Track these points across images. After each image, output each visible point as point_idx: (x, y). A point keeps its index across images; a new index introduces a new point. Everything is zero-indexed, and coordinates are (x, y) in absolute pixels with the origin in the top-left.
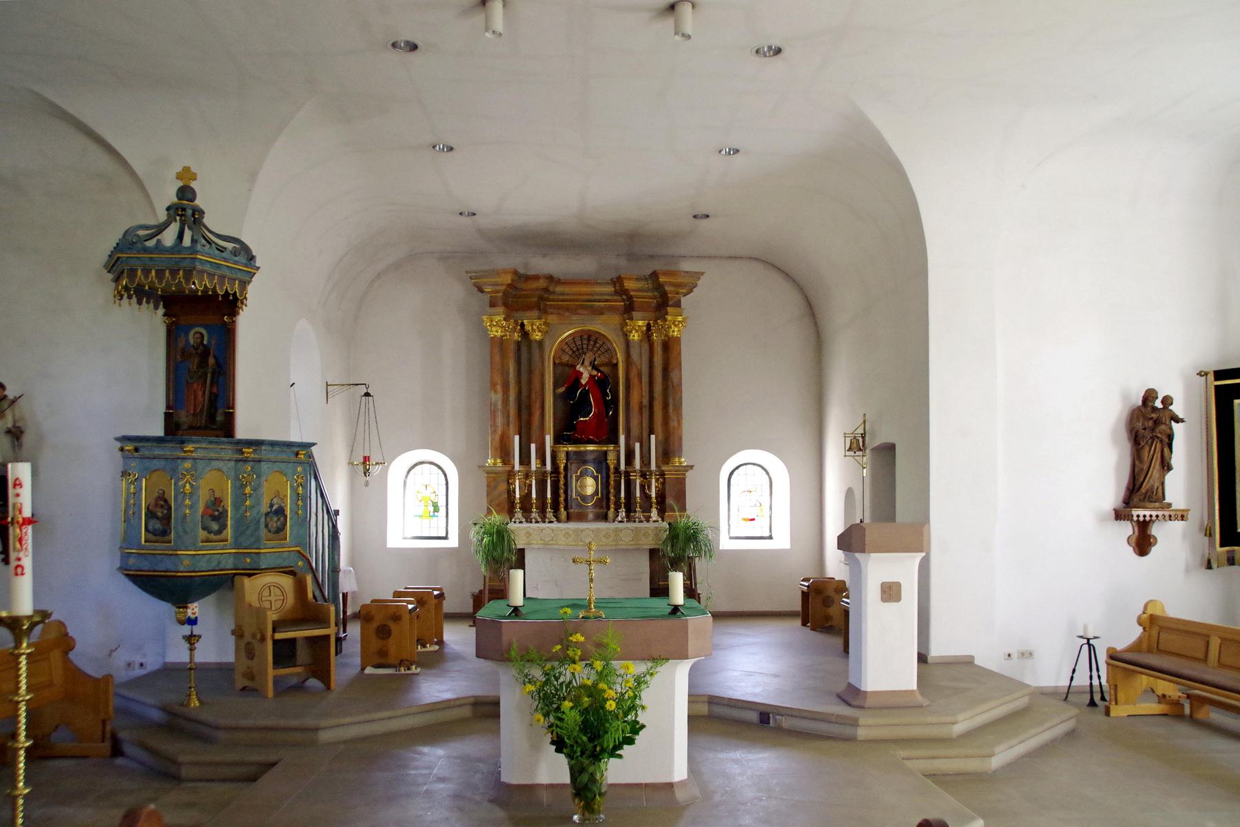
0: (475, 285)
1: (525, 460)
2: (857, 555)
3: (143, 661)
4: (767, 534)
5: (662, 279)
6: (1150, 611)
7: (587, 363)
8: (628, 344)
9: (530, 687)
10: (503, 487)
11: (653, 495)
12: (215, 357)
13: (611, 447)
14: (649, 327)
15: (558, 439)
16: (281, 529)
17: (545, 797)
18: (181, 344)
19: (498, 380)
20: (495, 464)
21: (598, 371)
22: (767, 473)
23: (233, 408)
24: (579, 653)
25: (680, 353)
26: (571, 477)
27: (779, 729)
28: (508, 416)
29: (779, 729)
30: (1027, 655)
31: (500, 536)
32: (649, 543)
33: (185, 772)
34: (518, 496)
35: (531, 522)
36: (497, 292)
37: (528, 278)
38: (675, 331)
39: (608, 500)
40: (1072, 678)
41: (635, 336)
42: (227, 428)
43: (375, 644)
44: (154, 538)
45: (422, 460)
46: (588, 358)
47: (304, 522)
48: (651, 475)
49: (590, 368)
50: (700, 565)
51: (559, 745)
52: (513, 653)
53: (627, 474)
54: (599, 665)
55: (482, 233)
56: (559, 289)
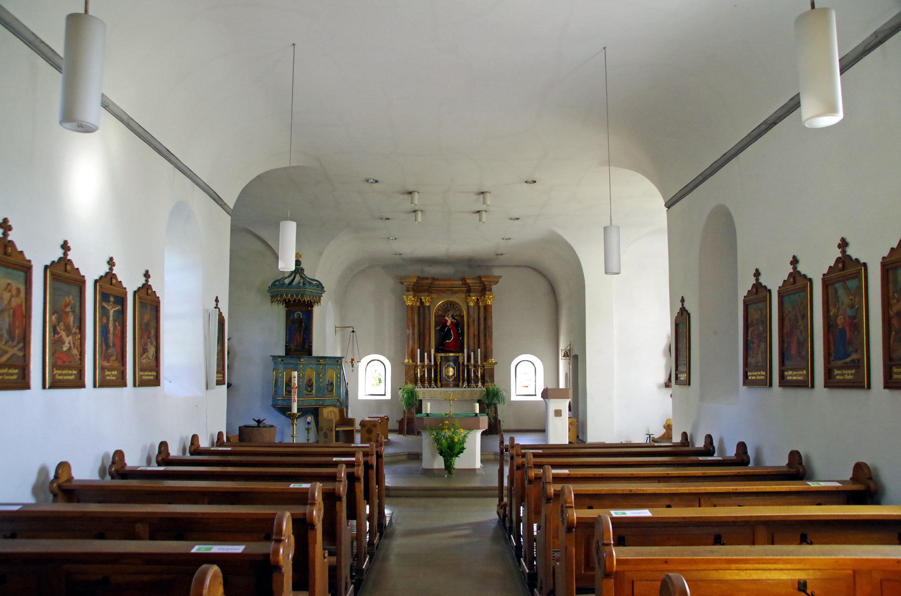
0: (400, 282)
1: (422, 360)
6: (668, 423)
7: (450, 316)
8: (468, 307)
9: (433, 436)
10: (412, 372)
11: (479, 376)
14: (478, 300)
15: (437, 351)
16: (332, 390)
17: (436, 472)
19: (410, 324)
20: (409, 361)
21: (455, 319)
22: (534, 365)
23: (312, 343)
24: (447, 427)
25: (491, 312)
28: (414, 340)
31: (412, 394)
34: (419, 376)
35: (425, 388)
36: (409, 285)
37: (424, 279)
38: (489, 302)
39: (459, 378)
41: (472, 304)
42: (309, 352)
44: (288, 394)
46: (450, 314)
47: (339, 387)
48: (478, 367)
50: (500, 407)
51: (441, 453)
52: (427, 426)
53: (468, 366)
54: (452, 430)
55: (404, 260)
56: (437, 283)
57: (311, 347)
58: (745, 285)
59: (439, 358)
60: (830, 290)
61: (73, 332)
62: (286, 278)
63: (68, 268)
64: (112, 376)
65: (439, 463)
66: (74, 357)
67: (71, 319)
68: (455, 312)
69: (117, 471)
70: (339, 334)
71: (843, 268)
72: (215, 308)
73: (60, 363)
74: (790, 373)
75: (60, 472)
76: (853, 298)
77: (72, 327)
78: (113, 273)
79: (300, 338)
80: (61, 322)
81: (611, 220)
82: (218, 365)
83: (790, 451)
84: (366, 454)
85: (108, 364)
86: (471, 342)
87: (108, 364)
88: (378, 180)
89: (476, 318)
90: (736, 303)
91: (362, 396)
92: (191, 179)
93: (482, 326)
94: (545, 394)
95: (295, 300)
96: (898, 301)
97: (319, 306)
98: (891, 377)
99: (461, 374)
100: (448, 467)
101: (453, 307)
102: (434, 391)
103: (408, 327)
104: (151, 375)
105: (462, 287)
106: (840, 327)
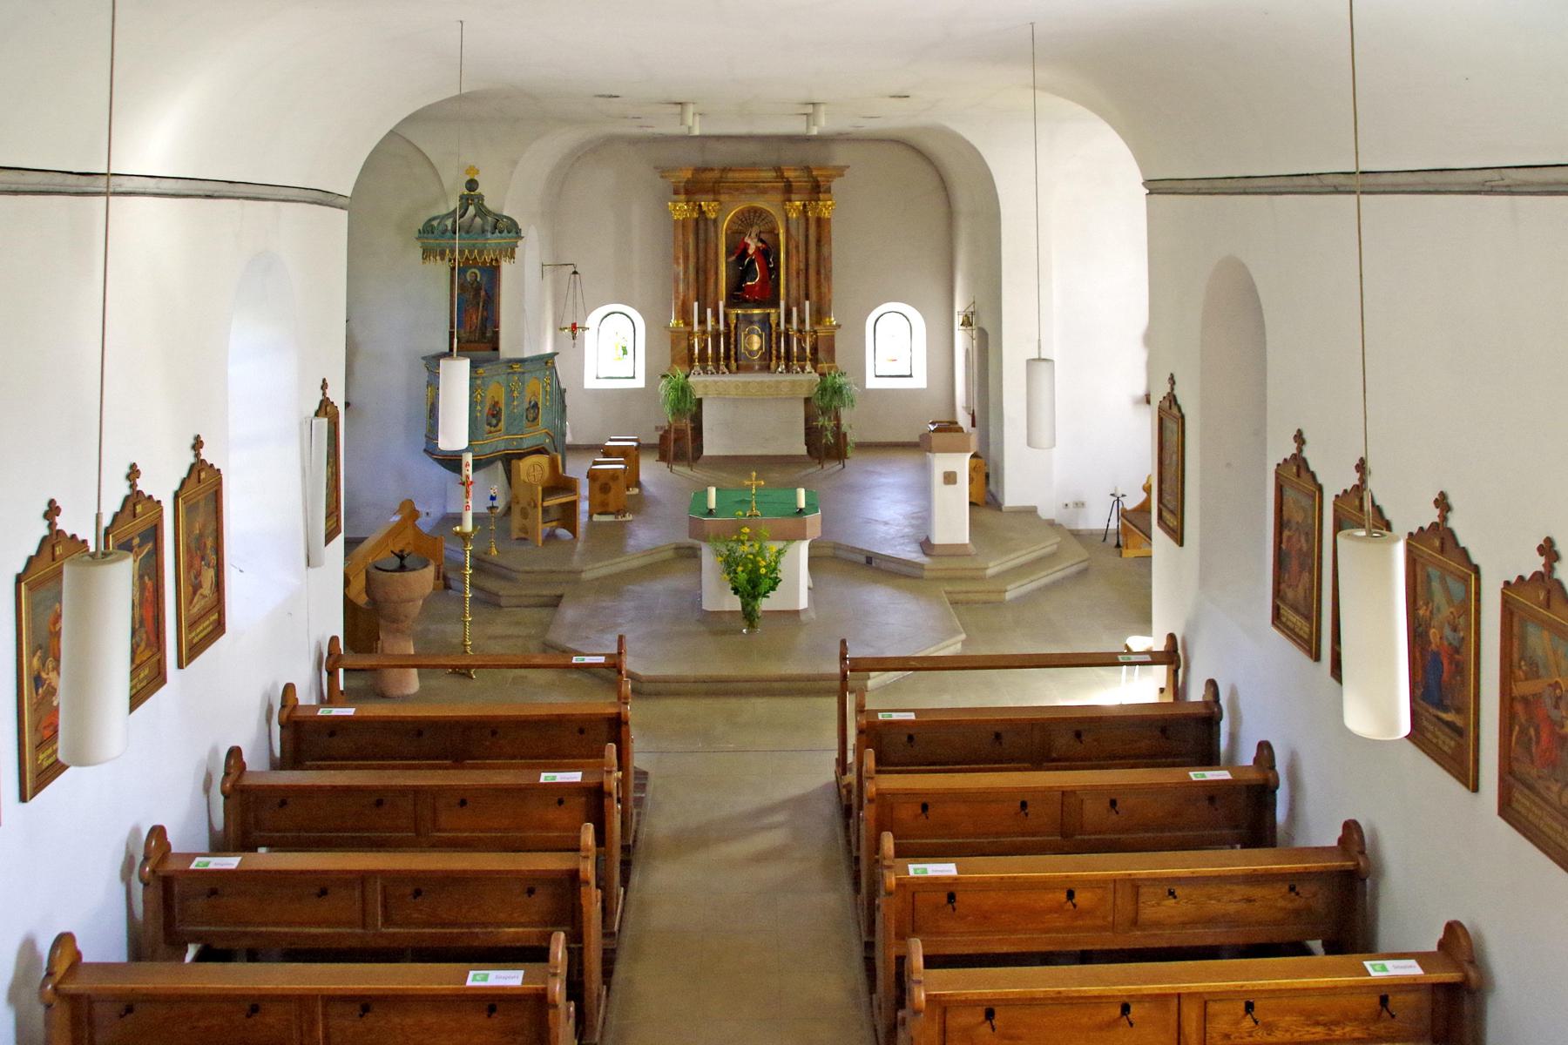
1: (702, 321)
2: (928, 454)
3: (428, 511)
4: (908, 374)
5: (815, 173)
7: (753, 235)
8: (787, 220)
10: (684, 344)
12: (486, 291)
13: (773, 311)
14: (804, 206)
15: (728, 305)
16: (535, 418)
20: (678, 324)
26: (740, 335)
27: (878, 569)
29: (878, 569)
30: (1080, 505)
31: (683, 390)
32: (804, 393)
33: (503, 602)
36: (679, 182)
38: (826, 214)
39: (771, 353)
40: (1108, 526)
43: (599, 497)
46: (755, 230)
49: (756, 240)
56: (730, 175)
59: (733, 321)
65: (734, 603)
68: (764, 225)
70: (548, 277)
79: (477, 319)
81: (1039, 347)
83: (1343, 823)
86: (793, 285)
89: (802, 239)
90: (1264, 470)
91: (590, 383)
99: (774, 346)
100: (749, 615)
101: (760, 217)
102: (725, 382)
103: (676, 259)
105: (777, 182)
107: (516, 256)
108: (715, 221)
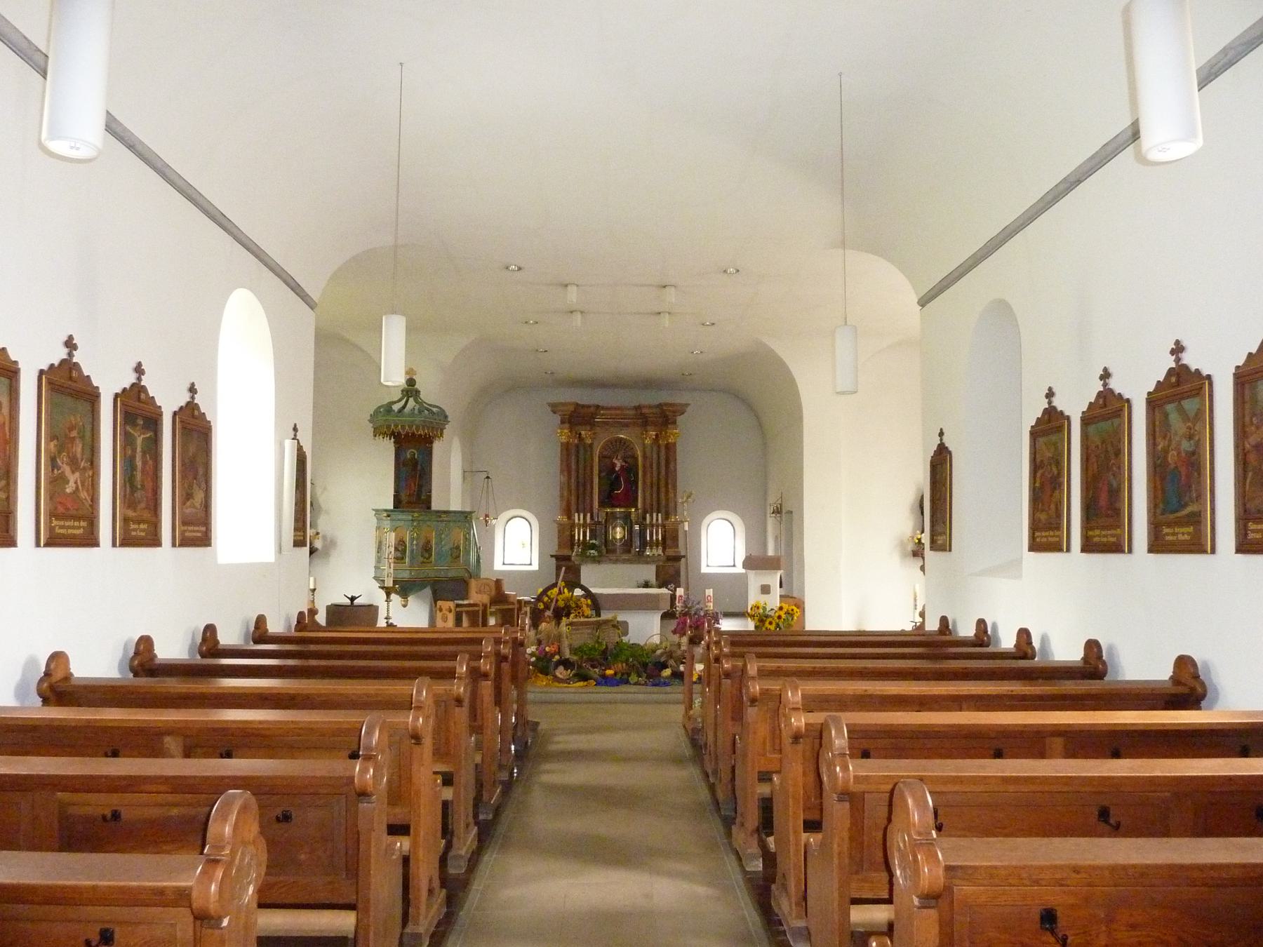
14: (657, 435)
18: (402, 459)
41: (648, 441)
42: (427, 504)
45: (529, 519)
47: (467, 553)
57: (430, 497)
58: (1033, 411)
60: (1158, 416)
61: (81, 467)
62: (395, 402)
63: (74, 375)
64: (140, 531)
66: (83, 503)
67: (78, 448)
69: (141, 665)
71: (1178, 384)
72: (293, 439)
73: (61, 509)
74: (1097, 532)
75: (52, 666)
76: (1192, 426)
77: (80, 460)
78: (142, 384)
80: (63, 452)
82: (296, 520)
84: (498, 641)
85: (134, 514)
87: (134, 514)
88: (522, 266)
92: (257, 256)
93: (663, 472)
94: (750, 563)
95: (408, 433)
96: (1258, 428)
97: (441, 442)
98: (1246, 534)
104: (198, 531)
106: (1172, 466)
107: (444, 436)
108: (591, 446)
